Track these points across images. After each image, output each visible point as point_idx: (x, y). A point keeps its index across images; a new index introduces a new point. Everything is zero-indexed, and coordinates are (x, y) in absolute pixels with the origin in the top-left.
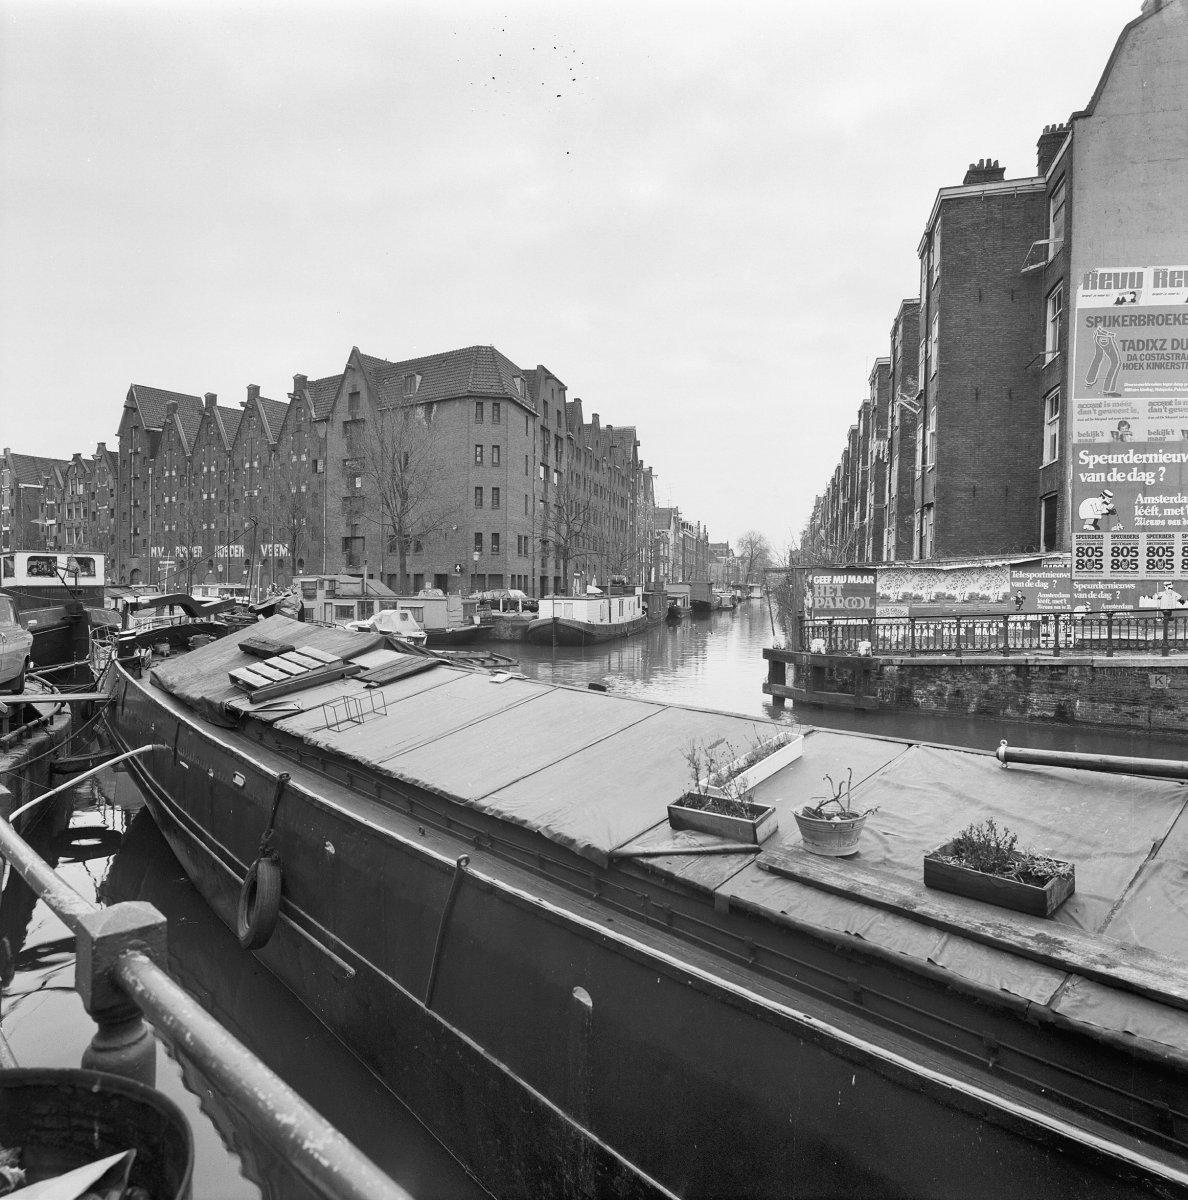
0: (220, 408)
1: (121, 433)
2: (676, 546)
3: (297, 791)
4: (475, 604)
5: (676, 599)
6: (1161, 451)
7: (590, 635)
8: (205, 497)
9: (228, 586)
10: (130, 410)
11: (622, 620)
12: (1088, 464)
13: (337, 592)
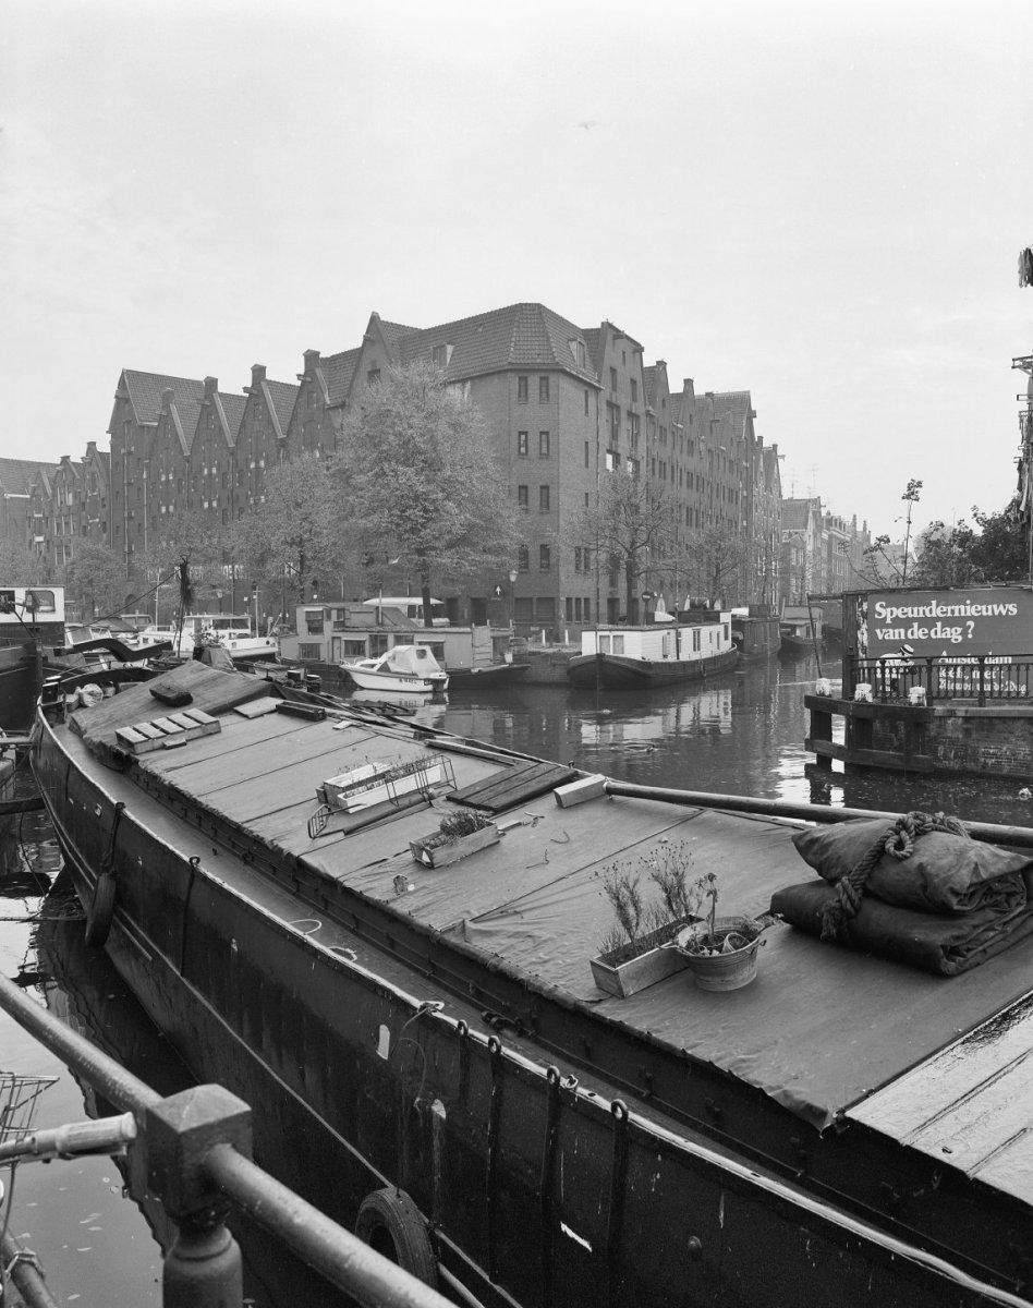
0: (222, 395)
1: (113, 430)
2: (817, 551)
3: (205, 878)
4: (508, 637)
5: (794, 627)
6: (968, 602)
7: (645, 676)
8: (206, 505)
9: (222, 616)
10: (122, 401)
11: (695, 656)
12: (886, 617)
13: (347, 624)
